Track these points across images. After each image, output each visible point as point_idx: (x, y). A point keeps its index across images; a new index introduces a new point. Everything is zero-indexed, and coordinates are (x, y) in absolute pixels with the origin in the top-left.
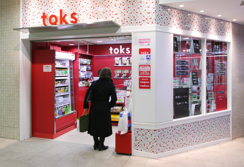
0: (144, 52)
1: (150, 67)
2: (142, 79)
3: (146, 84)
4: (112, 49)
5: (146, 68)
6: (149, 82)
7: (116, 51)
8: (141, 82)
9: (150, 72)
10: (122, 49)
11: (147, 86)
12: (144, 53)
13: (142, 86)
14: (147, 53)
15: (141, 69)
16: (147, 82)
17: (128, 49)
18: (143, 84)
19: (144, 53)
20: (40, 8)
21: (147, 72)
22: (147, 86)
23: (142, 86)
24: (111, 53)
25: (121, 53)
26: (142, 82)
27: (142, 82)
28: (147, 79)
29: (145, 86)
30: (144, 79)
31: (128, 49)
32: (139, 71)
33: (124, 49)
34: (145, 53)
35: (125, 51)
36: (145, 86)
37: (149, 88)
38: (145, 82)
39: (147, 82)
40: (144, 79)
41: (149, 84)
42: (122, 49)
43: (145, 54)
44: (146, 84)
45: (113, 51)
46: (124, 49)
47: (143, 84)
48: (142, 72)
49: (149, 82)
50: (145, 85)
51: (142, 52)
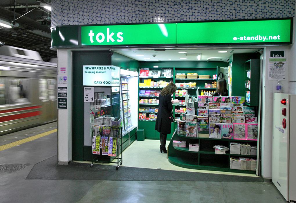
0: (100, 34)
1: (67, 89)
2: (61, 100)
3: (64, 105)
4: (93, 34)
5: (63, 90)
6: (66, 103)
7: (100, 38)
8: (59, 103)
9: (66, 93)
10: (110, 33)
11: (64, 106)
12: (276, 56)
13: (61, 106)
14: (280, 56)
15: (59, 91)
16: (64, 103)
17: (120, 35)
18: (61, 104)
19: (276, 56)
20: (113, 8)
21: (65, 93)
22: (64, 106)
23: (61, 106)
24: (92, 41)
25: (108, 41)
26: (60, 103)
27: (60, 103)
28: (64, 100)
29: (63, 106)
30: (63, 100)
31: (120, 35)
32: (58, 93)
33: (113, 34)
34: (278, 56)
35: (115, 37)
36: (63, 106)
37: (66, 108)
38: (63, 103)
39: (64, 103)
40: (63, 100)
41: (66, 105)
42: (110, 33)
43: (277, 57)
44: (64, 105)
45: (94, 38)
46: (113, 34)
47: (61, 104)
48: (60, 93)
49: (66, 103)
50: (63, 105)
51: (273, 55)
